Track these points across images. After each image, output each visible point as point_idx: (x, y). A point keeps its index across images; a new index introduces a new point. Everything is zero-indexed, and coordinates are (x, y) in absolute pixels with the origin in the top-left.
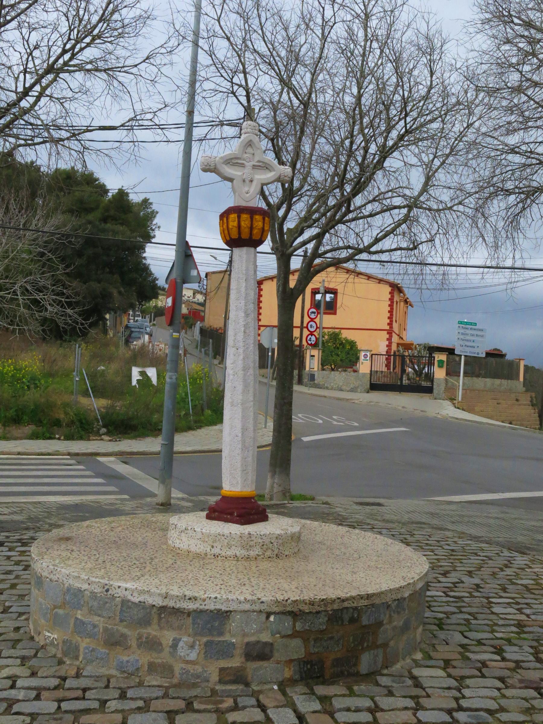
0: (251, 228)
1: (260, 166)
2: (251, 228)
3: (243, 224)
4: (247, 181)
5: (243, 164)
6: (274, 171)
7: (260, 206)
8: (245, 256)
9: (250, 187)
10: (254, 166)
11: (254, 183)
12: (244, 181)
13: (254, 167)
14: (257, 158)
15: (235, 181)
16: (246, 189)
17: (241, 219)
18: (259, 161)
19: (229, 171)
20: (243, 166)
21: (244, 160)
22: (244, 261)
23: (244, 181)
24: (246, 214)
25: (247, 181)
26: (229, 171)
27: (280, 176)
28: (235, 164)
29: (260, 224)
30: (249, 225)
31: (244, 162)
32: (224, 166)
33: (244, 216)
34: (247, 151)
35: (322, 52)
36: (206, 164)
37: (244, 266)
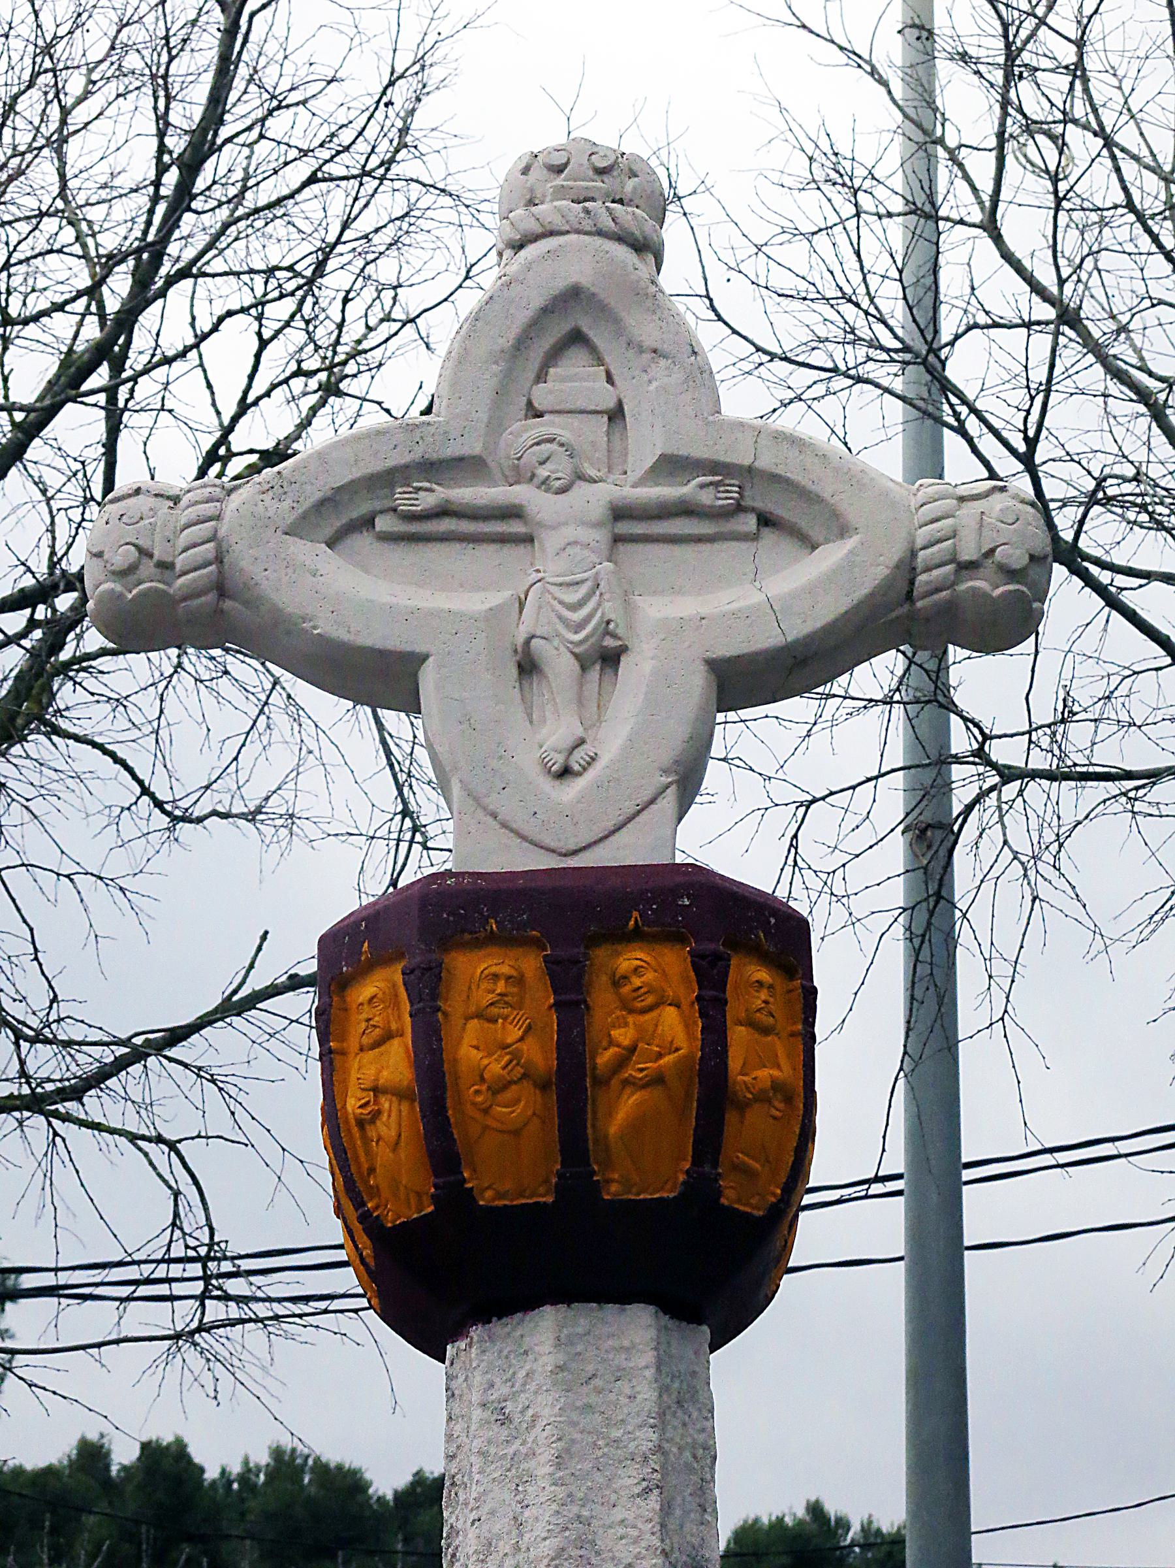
0: (572, 1083)
1: (686, 510)
2: (572, 1083)
3: (470, 1050)
4: (560, 664)
5: (513, 512)
6: (844, 531)
7: (781, 893)
8: (546, 1406)
9: (592, 713)
10: (620, 513)
11: (637, 669)
12: (528, 667)
13: (628, 524)
14: (646, 443)
15: (428, 680)
16: (557, 732)
17: (454, 1005)
18: (671, 465)
19: (360, 592)
20: (507, 528)
21: (518, 475)
22: (542, 1468)
23: (528, 667)
24: (505, 940)
25: (560, 664)
26: (360, 592)
27: (908, 568)
28: (422, 530)
29: (675, 1029)
30: (540, 1055)
31: (521, 493)
32: (309, 552)
33: (481, 973)
34: (542, 396)
35: (77, 738)
36: (122, 557)
37: (541, 1517)
